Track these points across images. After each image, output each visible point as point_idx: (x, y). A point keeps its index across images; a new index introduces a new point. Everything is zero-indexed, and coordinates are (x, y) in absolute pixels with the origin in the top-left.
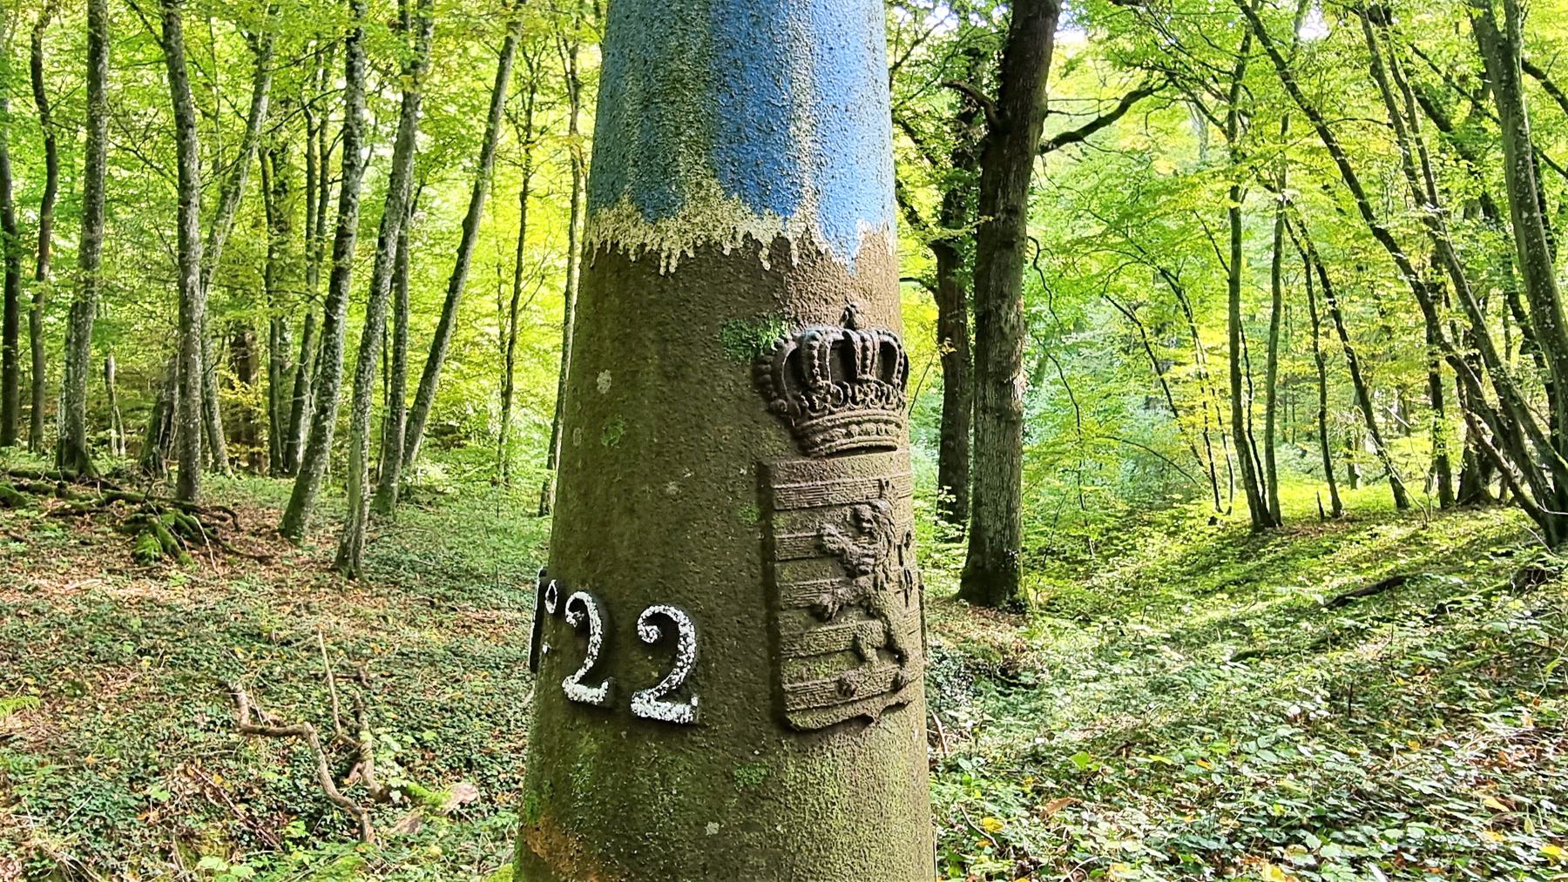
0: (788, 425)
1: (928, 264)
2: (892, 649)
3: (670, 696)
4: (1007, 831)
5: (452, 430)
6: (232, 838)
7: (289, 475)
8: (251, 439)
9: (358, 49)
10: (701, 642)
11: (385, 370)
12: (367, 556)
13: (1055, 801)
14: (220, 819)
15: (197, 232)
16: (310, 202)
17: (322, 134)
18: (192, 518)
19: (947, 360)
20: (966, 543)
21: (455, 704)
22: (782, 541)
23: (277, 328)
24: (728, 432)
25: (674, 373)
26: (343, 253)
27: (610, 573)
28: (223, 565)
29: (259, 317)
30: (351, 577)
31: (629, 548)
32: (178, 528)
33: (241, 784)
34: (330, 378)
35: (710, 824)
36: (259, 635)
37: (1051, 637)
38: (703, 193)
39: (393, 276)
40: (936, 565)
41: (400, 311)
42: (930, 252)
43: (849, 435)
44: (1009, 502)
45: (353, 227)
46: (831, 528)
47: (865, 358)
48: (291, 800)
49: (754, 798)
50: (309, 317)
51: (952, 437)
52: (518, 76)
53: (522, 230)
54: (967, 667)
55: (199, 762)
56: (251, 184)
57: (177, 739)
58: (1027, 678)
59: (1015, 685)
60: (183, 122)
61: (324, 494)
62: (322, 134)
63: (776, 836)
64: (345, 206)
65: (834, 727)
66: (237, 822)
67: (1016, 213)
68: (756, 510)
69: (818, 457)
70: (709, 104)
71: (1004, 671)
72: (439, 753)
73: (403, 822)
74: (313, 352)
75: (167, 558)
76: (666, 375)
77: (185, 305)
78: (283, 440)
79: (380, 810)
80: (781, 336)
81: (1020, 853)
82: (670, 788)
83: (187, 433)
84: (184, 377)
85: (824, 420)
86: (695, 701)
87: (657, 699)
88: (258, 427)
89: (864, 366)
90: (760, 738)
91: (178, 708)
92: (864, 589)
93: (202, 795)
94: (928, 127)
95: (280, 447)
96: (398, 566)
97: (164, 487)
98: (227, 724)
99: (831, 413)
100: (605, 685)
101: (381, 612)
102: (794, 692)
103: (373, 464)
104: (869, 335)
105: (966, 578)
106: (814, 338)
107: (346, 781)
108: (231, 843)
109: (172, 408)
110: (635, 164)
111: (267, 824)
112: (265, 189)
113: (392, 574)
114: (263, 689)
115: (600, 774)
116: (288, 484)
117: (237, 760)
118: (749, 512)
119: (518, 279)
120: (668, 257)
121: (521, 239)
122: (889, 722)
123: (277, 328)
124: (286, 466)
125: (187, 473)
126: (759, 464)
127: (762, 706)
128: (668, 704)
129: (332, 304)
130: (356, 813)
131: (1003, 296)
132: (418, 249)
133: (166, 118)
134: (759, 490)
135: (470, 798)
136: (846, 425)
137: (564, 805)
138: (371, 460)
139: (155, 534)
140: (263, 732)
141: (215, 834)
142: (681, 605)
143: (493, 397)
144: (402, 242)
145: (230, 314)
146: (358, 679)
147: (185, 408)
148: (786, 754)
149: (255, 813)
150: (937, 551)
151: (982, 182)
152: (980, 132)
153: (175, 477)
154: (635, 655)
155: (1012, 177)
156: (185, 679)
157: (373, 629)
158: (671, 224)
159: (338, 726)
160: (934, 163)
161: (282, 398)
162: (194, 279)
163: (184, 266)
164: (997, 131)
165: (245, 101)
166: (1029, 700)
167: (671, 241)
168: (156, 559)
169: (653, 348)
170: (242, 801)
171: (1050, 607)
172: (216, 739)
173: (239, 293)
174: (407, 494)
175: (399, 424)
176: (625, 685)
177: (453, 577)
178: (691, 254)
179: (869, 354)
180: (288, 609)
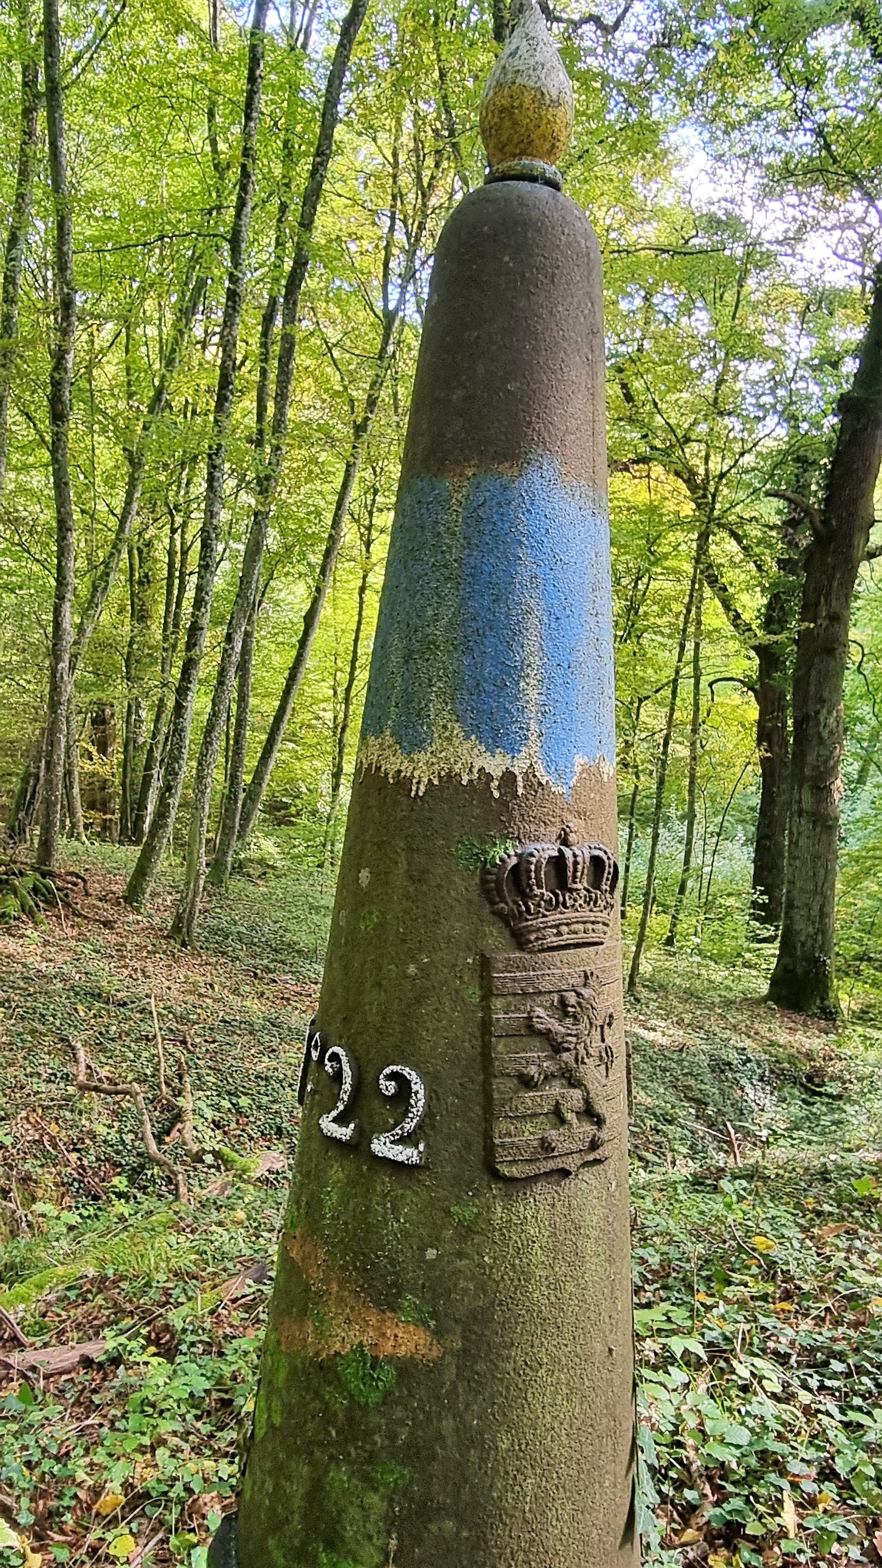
0: (508, 925)
1: (748, 665)
2: (590, 1113)
3: (402, 1140)
4: (777, 1253)
5: (286, 806)
6: (63, 1184)
7: (137, 843)
8: (104, 807)
9: (218, 462)
10: (429, 1098)
11: (227, 750)
12: (200, 925)
13: (832, 1225)
14: (55, 1165)
15: (70, 619)
16: (169, 592)
17: (183, 532)
18: (48, 881)
19: (764, 761)
20: (777, 944)
21: (270, 1073)
22: (498, 1020)
23: (133, 708)
24: (459, 928)
25: (417, 877)
26: (195, 645)
27: (361, 1033)
28: (72, 926)
29: (119, 692)
30: (184, 945)
31: (377, 1013)
32: (35, 890)
33: (74, 1134)
34: (177, 759)
35: (430, 1250)
36: (99, 995)
37: (861, 1048)
38: (447, 734)
39: (239, 665)
40: (747, 965)
41: (243, 699)
42: (753, 654)
43: (559, 934)
44: (822, 907)
45: (205, 621)
46: (540, 1011)
47: (575, 870)
48: (118, 1152)
49: (467, 1231)
50: (161, 700)
51: (768, 837)
52: (363, 480)
53: (359, 623)
54: (772, 1072)
55: (40, 1111)
56: (118, 578)
57: (22, 1088)
58: (833, 1088)
59: (820, 1094)
60: (63, 526)
61: (166, 864)
62: (183, 532)
63: (482, 1266)
64: (199, 603)
65: (536, 1178)
66: (69, 1170)
67: (838, 620)
68: (478, 992)
69: (531, 952)
70: (456, 664)
71: (810, 1079)
72: (252, 1119)
73: (215, 1184)
74: (165, 729)
75: (24, 917)
76: (411, 877)
77: (55, 689)
78: (132, 810)
79: (195, 1169)
80: (505, 853)
81: (788, 1278)
82: (401, 1217)
83: (49, 804)
84: (50, 753)
85: (538, 922)
86: (421, 1147)
87: (392, 1142)
88: (111, 797)
89: (575, 877)
90: (473, 1182)
91: (25, 1058)
92: (566, 1063)
93: (40, 1142)
94: (754, 531)
95: (126, 815)
96: (227, 937)
97: (25, 854)
98: (66, 1077)
99: (544, 916)
100: (352, 1126)
101: (209, 980)
102: (503, 1145)
103: (211, 835)
104: (581, 851)
105: (775, 982)
106: (532, 855)
107: (167, 1139)
108: (62, 1189)
109: (37, 779)
110: (397, 706)
111: (95, 1174)
112: (131, 580)
113: (220, 943)
114: (98, 1046)
115: (344, 1199)
116: (135, 852)
117: (72, 1111)
118: (473, 994)
119: (353, 668)
120: (418, 783)
121: (358, 630)
122: (587, 1174)
123: (133, 708)
124: (134, 834)
125: (46, 841)
126: (483, 956)
127: (475, 1157)
128: (400, 1147)
129: (182, 691)
130: (172, 1172)
131: (822, 701)
132: (264, 638)
133: (48, 516)
134: (482, 977)
135: (278, 1166)
136: (557, 926)
137: (316, 1221)
138: (208, 831)
139: (15, 894)
140: (96, 1089)
141: (49, 1179)
142: (415, 1067)
143: (325, 777)
144: (248, 635)
145: (94, 695)
146: (184, 1042)
147: (49, 782)
148: (494, 1197)
149: (85, 1163)
150: (749, 950)
151: (805, 588)
152: (805, 539)
153: (36, 841)
154: (376, 1103)
155: (835, 584)
156: (33, 1032)
157: (200, 995)
158: (422, 757)
159: (163, 1086)
160: (759, 568)
161: (133, 770)
162: (64, 665)
163: (55, 654)
164: (822, 541)
165: (118, 503)
166: (832, 1111)
167: (422, 770)
168: (15, 919)
169: (403, 854)
170: (75, 1150)
171: (863, 1016)
172: (55, 1090)
173: (102, 677)
174: (240, 867)
175: (236, 802)
176: (367, 1127)
177: (276, 951)
178: (436, 782)
179: (580, 867)
180: (126, 972)
